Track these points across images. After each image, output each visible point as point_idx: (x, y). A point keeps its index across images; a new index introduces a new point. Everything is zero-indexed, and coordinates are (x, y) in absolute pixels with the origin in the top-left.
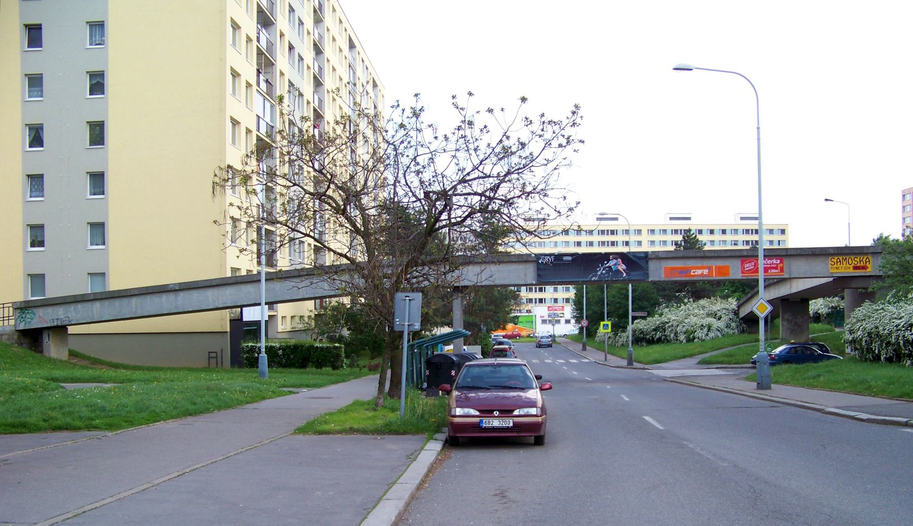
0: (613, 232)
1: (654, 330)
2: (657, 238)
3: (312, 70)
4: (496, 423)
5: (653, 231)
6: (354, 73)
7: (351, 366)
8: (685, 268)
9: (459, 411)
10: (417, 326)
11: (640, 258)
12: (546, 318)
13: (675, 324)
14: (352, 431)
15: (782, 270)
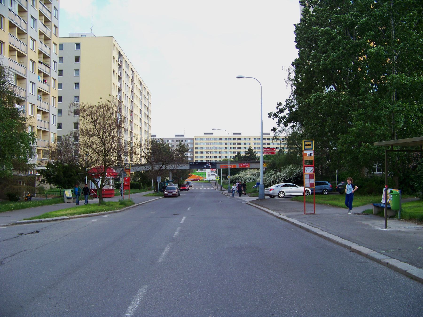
0: (239, 139)
1: (235, 179)
2: (257, 141)
3: (118, 62)
4: (170, 194)
5: (255, 139)
6: (142, 93)
7: (143, 189)
8: (225, 166)
9: (165, 193)
10: (160, 181)
11: (214, 163)
12: (210, 173)
13: (242, 177)
14: (151, 196)
15: (249, 166)
